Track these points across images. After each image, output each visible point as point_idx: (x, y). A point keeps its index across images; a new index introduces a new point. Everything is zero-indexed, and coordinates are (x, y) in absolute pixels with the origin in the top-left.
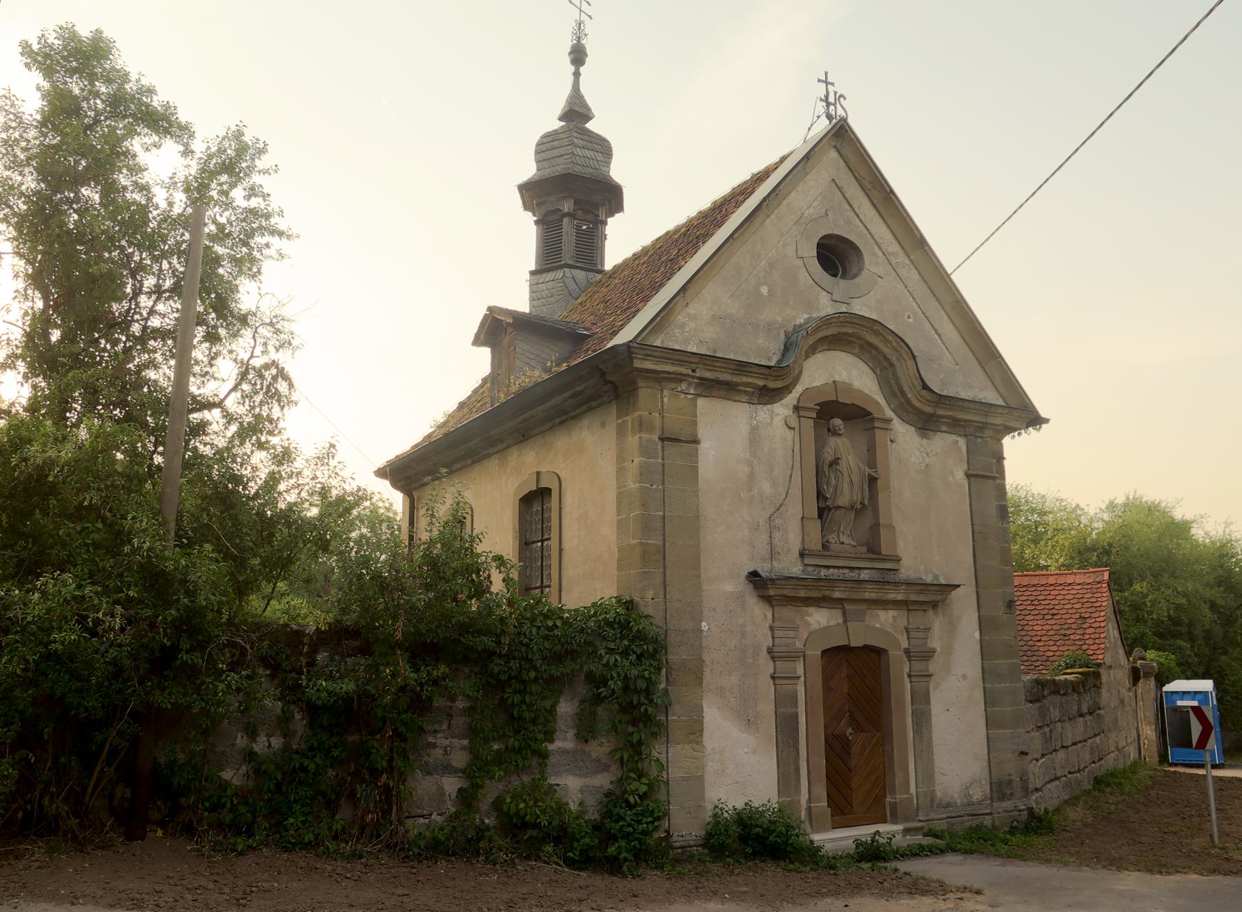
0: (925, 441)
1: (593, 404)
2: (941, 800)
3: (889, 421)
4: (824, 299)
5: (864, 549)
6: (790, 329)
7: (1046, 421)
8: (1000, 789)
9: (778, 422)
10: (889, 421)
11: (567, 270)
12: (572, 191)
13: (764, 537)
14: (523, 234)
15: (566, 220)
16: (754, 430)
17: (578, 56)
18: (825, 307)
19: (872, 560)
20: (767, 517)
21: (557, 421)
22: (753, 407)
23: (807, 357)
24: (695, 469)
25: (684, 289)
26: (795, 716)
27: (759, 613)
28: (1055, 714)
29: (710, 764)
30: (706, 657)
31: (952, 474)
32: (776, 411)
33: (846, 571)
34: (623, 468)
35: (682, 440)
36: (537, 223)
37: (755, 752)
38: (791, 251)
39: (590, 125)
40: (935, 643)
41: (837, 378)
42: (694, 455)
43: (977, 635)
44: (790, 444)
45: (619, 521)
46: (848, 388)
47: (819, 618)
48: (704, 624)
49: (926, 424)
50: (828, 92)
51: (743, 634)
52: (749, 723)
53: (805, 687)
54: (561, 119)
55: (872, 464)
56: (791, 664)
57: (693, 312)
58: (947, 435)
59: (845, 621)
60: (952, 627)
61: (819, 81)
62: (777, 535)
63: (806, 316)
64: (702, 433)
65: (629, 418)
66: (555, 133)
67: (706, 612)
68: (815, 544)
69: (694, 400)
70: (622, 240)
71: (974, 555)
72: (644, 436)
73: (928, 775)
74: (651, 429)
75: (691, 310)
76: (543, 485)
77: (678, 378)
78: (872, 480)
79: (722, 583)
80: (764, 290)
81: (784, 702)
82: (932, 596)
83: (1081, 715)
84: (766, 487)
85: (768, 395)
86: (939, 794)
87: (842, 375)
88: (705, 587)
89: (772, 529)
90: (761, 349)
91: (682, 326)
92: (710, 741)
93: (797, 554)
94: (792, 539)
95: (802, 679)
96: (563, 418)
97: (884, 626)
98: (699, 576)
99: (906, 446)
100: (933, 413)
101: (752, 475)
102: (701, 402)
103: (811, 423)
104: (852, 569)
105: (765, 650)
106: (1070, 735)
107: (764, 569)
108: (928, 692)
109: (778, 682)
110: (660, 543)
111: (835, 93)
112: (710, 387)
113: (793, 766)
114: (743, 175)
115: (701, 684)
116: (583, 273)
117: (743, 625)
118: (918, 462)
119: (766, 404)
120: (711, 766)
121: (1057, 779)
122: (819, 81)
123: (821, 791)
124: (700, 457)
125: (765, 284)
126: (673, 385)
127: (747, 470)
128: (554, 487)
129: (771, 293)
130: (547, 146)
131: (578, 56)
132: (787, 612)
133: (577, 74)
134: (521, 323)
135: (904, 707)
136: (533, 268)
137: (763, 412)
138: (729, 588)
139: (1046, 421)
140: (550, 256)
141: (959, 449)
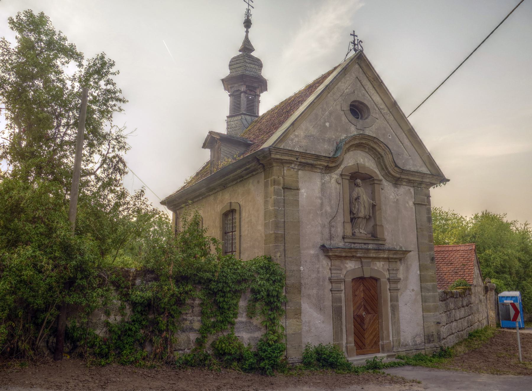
0: (396, 189)
1: (254, 173)
3: (381, 180)
5: (370, 236)
9: (333, 181)
10: (381, 180)
11: (243, 116)
13: (327, 230)
14: (224, 100)
16: (323, 184)
17: (248, 24)
18: (353, 131)
20: (328, 221)
21: (239, 180)
23: (346, 153)
24: (297, 201)
26: (341, 307)
27: (325, 263)
28: (452, 306)
30: (302, 282)
36: (230, 95)
38: (338, 107)
39: (252, 54)
42: (297, 195)
43: (418, 272)
44: (338, 190)
45: (265, 224)
46: (364, 167)
47: (351, 265)
48: (301, 267)
49: (397, 182)
50: (355, 40)
51: (318, 272)
52: (321, 309)
54: (240, 51)
56: (339, 285)
58: (406, 187)
59: (362, 266)
60: (407, 269)
61: (351, 35)
64: (300, 185)
65: (270, 179)
67: (302, 262)
68: (349, 232)
70: (267, 103)
71: (417, 238)
72: (276, 187)
73: (398, 332)
74: (279, 184)
77: (290, 162)
78: (374, 206)
79: (310, 251)
80: (327, 124)
81: (336, 300)
82: (398, 256)
83: (463, 307)
84: (328, 209)
86: (402, 340)
87: (361, 161)
88: (302, 252)
89: (331, 226)
90: (325, 149)
91: (292, 140)
92: (305, 318)
93: (341, 238)
95: (344, 291)
97: (380, 267)
98: (299, 247)
101: (322, 204)
104: (365, 244)
107: (327, 244)
108: (397, 297)
110: (283, 233)
111: (358, 40)
112: (304, 166)
113: (340, 328)
117: (318, 268)
120: (305, 328)
121: (453, 334)
122: (351, 35)
125: (328, 122)
126: (288, 165)
127: (320, 201)
129: (330, 126)
131: (248, 24)
133: (247, 32)
138: (312, 252)
141: (411, 193)
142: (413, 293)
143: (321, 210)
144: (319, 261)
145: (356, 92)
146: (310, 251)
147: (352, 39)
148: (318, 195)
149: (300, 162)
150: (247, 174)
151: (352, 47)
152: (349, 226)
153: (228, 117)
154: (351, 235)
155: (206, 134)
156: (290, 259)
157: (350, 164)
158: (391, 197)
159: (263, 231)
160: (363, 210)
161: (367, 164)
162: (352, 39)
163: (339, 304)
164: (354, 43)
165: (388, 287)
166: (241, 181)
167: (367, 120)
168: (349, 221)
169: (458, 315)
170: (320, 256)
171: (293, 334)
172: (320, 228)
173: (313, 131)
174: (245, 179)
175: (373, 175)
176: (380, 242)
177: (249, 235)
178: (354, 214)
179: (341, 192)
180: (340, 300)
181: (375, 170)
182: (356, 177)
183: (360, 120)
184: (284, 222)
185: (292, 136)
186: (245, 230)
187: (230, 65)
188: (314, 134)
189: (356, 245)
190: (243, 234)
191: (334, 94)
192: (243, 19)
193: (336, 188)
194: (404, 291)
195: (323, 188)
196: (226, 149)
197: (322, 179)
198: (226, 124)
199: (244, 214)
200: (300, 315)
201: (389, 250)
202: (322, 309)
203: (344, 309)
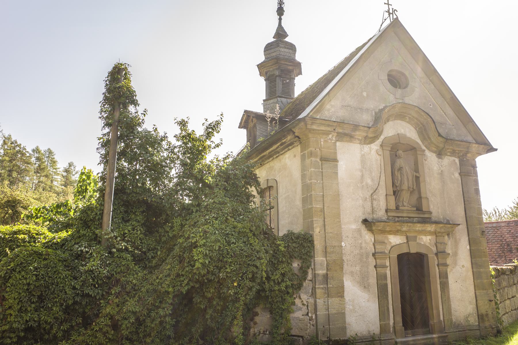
0: (440, 160)
1: (290, 147)
3: (424, 151)
4: (391, 97)
5: (415, 209)
6: (377, 110)
7: (496, 150)
8: (481, 317)
9: (373, 152)
10: (424, 151)
11: (279, 98)
12: (279, 64)
13: (369, 204)
14: (260, 85)
15: (277, 78)
16: (363, 156)
17: (280, 11)
18: (391, 99)
19: (419, 213)
20: (370, 194)
21: (275, 156)
22: (362, 146)
23: (385, 123)
25: (328, 93)
26: (386, 285)
27: (368, 237)
28: (504, 284)
29: (348, 306)
30: (344, 258)
31: (453, 175)
32: (372, 147)
34: (304, 174)
35: (331, 160)
36: (265, 80)
37: (368, 301)
39: (287, 39)
40: (449, 251)
41: (399, 132)
42: (336, 166)
43: (468, 247)
44: (379, 162)
45: (303, 198)
46: (405, 136)
47: (395, 240)
48: (343, 243)
50: (389, 9)
51: (361, 248)
52: (365, 287)
53: (391, 271)
54: (274, 38)
55: (417, 170)
56: (383, 261)
57: (333, 104)
58: (450, 158)
59: (408, 242)
61: (385, 4)
62: (375, 203)
63: (384, 105)
64: (339, 157)
65: (306, 152)
66: (273, 42)
67: (344, 238)
68: (392, 206)
69: (335, 143)
70: (301, 85)
71: (465, 211)
72: (313, 159)
74: (316, 156)
75: (332, 103)
76: (269, 185)
78: (417, 178)
79: (350, 224)
80: (365, 94)
81: (381, 278)
83: (514, 284)
84: (369, 181)
85: (369, 140)
86: (454, 320)
87: (402, 131)
88: (343, 226)
89: (372, 200)
92: (348, 296)
94: (381, 204)
95: (389, 268)
96: (277, 155)
97: (426, 241)
98: (340, 222)
99: (431, 162)
100: (445, 145)
101: (362, 176)
102: (338, 144)
105: (371, 255)
106: (511, 293)
107: (370, 218)
108: (447, 274)
109: (378, 269)
110: (321, 207)
111: (393, 9)
113: (386, 308)
114: (353, 49)
115: (343, 270)
116: (286, 99)
117: (361, 244)
120: (349, 307)
121: (507, 313)
122: (385, 4)
123: (399, 319)
124: (339, 168)
126: (324, 136)
127: (360, 174)
128: (275, 186)
130: (268, 48)
131: (280, 11)
132: (380, 237)
133: (280, 19)
134: (260, 118)
136: (265, 98)
137: (366, 148)
138: (354, 226)
139: (496, 150)
140: (272, 93)
141: (456, 163)
143: (362, 183)
144: (361, 236)
146: (350, 224)
147: (386, 8)
149: (337, 133)
150: (283, 149)
151: (387, 15)
152: (392, 199)
153: (264, 101)
154: (395, 208)
155: (243, 113)
156: (331, 234)
159: (301, 205)
160: (406, 183)
161: (408, 135)
162: (386, 8)
163: (385, 282)
164: (388, 12)
165: (436, 263)
166: (277, 157)
167: (406, 89)
168: (392, 194)
169: (511, 293)
170: (363, 231)
171: (336, 314)
172: (361, 202)
174: (281, 154)
175: (415, 146)
176: (426, 216)
177: (287, 211)
178: (397, 186)
179: (382, 164)
183: (399, 90)
184: (323, 195)
186: (283, 206)
187: (264, 51)
190: (280, 211)
192: (276, 7)
193: (377, 160)
194: (454, 267)
195: (363, 161)
196: (261, 127)
197: (361, 150)
198: (263, 107)
199: (280, 191)
200: (344, 294)
201: (436, 223)
202: (366, 286)
203: (389, 286)
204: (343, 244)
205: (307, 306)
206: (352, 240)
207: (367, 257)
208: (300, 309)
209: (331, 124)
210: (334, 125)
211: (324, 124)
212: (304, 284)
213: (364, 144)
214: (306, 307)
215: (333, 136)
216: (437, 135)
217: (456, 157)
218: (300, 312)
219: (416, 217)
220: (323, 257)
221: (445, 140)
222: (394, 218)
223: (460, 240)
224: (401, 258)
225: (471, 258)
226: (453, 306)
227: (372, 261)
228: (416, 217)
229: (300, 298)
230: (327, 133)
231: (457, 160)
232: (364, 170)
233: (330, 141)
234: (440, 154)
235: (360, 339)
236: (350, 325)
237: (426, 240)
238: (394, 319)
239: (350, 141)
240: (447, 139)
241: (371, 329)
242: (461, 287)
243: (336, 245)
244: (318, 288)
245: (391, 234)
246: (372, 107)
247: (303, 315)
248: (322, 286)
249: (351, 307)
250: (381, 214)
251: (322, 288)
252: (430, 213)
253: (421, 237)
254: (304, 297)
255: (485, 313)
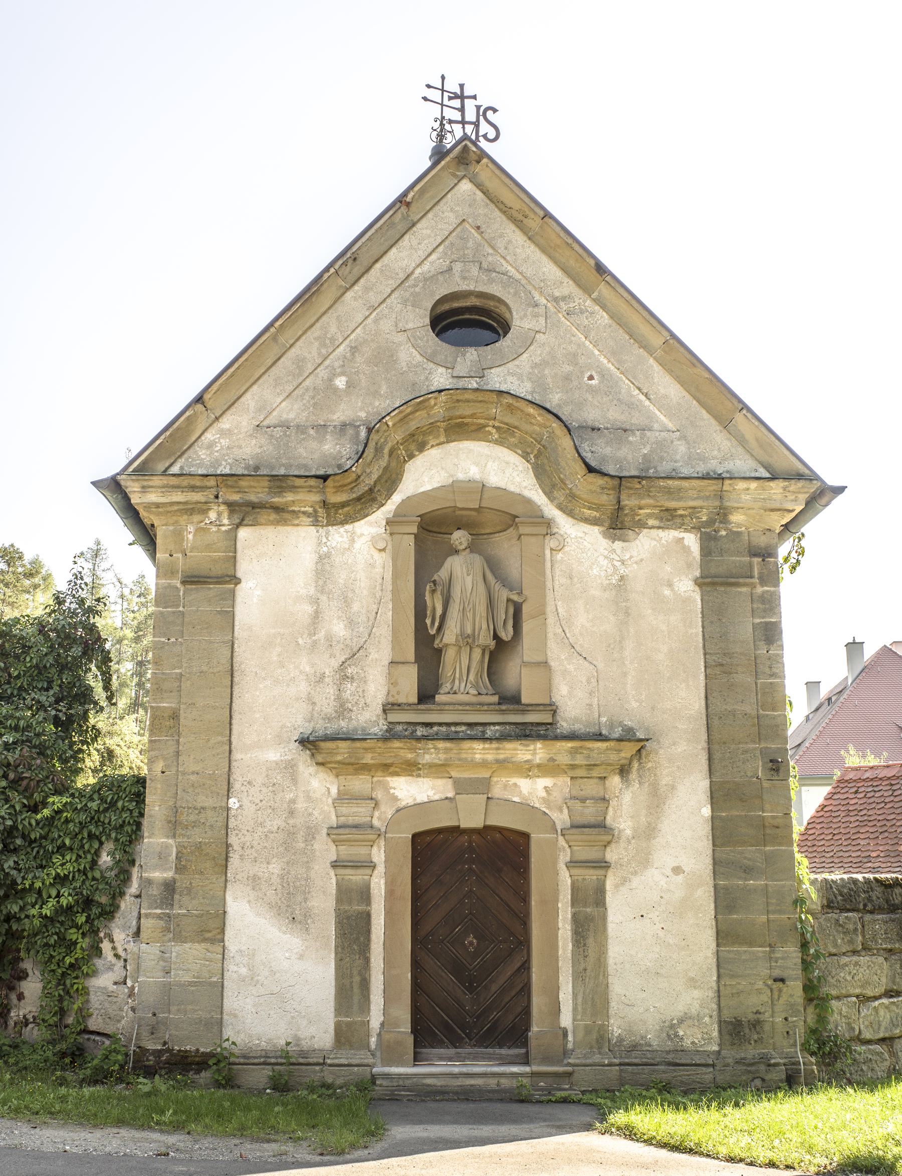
0: (618, 545)
2: (620, 1040)
7: (841, 490)
9: (362, 544)
13: (331, 691)
16: (323, 559)
20: (335, 663)
24: (230, 617)
26: (367, 917)
27: (319, 786)
30: (232, 839)
31: (670, 585)
33: (464, 728)
37: (301, 957)
43: (707, 811)
44: (379, 570)
47: (410, 790)
51: (291, 813)
53: (385, 882)
60: (657, 800)
64: (243, 568)
68: (409, 690)
80: (341, 382)
82: (628, 747)
84: (339, 629)
86: (617, 1032)
93: (379, 710)
97: (529, 789)
101: (317, 616)
103: (411, 540)
105: (325, 831)
112: (246, 512)
113: (357, 979)
117: (293, 801)
118: (610, 609)
119: (343, 523)
120: (235, 970)
125: (343, 374)
126: (196, 518)
127: (309, 609)
129: (349, 385)
132: (360, 783)
135: (548, 1065)
137: (338, 536)
138: (273, 755)
139: (841, 490)
141: (687, 550)
142: (680, 878)
144: (294, 780)
145: (458, 267)
148: (303, 592)
154: (414, 699)
156: (193, 778)
157: (428, 487)
158: (595, 571)
161: (495, 479)
170: (301, 767)
171: (191, 984)
172: (303, 687)
173: (290, 411)
180: (365, 895)
181: (527, 493)
182: (435, 532)
185: (209, 436)
188: (292, 416)
189: (435, 728)
191: (367, 289)
194: (635, 873)
195: (323, 565)
197: (319, 544)
202: (299, 918)
204: (233, 803)
205: (125, 960)
206: (264, 790)
207: (311, 834)
208: (110, 968)
209: (197, 482)
210: (208, 484)
211: (178, 487)
212: (123, 905)
213: (330, 523)
214: (122, 963)
215: (219, 514)
216: (581, 469)
217: (686, 530)
218: (110, 974)
219: (494, 724)
220: (168, 837)
221: (616, 482)
222: (410, 729)
223: (673, 788)
224: (526, 836)
225: (714, 845)
226: (618, 988)
227: (326, 851)
228: (494, 724)
229: (112, 941)
230: (201, 509)
231: (692, 541)
232: (324, 598)
233: (214, 529)
234: (618, 524)
235: (261, 1057)
236: (235, 1016)
237: (533, 789)
238: (386, 1009)
239: (283, 522)
240: (620, 478)
241: (302, 1034)
242: (661, 934)
243: (206, 804)
244: (147, 916)
245: (397, 774)
246: (363, 415)
247: (116, 983)
248: (159, 911)
249: (244, 971)
250: (368, 717)
251: (159, 917)
252: (552, 708)
253: (513, 780)
254: (119, 936)
255: (751, 1017)
